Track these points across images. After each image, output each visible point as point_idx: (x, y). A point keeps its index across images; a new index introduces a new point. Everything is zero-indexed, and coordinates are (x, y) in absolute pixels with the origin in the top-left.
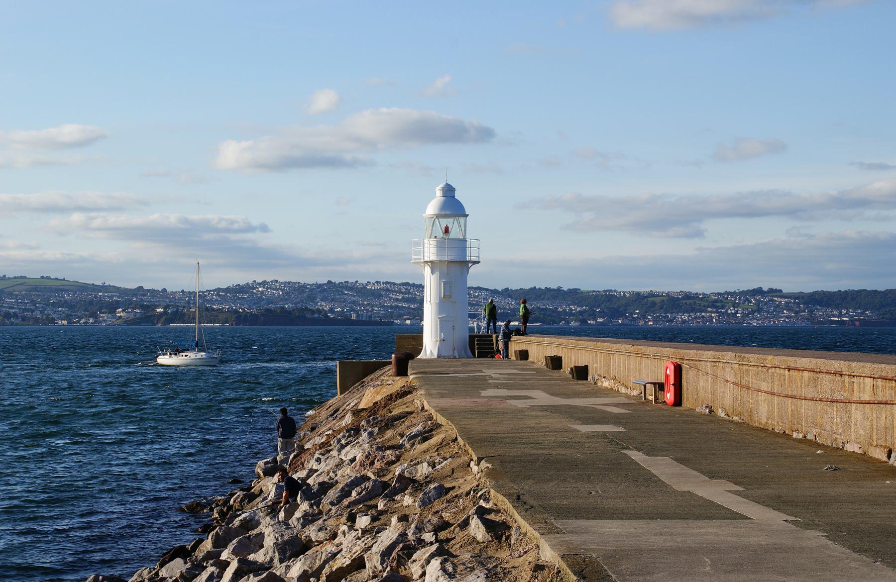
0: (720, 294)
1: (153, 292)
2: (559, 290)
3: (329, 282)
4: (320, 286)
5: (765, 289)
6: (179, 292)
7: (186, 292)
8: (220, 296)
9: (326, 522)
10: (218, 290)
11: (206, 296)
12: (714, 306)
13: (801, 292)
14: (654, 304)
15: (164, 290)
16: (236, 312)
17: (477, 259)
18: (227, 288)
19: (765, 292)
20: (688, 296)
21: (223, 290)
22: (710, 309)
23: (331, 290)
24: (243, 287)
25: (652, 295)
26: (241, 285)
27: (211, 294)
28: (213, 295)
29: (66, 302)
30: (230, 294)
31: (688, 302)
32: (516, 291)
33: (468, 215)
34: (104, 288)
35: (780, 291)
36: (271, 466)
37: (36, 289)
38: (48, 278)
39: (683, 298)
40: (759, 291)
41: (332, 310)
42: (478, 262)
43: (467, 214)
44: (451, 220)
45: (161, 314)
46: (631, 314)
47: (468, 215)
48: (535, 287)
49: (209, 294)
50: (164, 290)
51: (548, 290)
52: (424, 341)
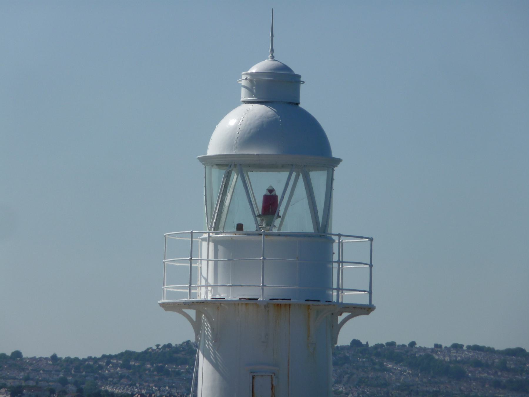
6: (46, 359)
7: (60, 359)
8: (129, 367)
9: (331, 169)
10: (128, 356)
11: (101, 367)
15: (17, 354)
17: (362, 299)
18: (146, 352)
23: (244, 187)
26: (173, 345)
27: (113, 364)
28: (115, 366)
30: (152, 364)
36: (138, 365)
42: (367, 309)
43: (365, 343)
44: (284, 175)
49: (108, 363)
50: (17, 354)
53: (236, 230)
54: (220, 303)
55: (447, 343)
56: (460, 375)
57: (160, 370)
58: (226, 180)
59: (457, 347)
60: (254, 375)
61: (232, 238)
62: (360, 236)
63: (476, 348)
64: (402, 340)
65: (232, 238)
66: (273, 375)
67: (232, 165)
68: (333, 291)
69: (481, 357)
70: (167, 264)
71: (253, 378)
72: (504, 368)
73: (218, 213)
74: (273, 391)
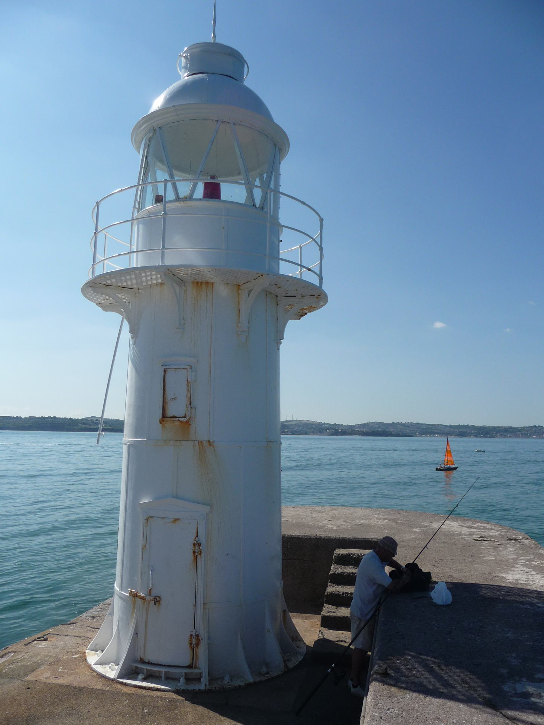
0: (522, 427)
1: (339, 425)
2: (468, 425)
3: (393, 422)
4: (390, 424)
5: (537, 426)
12: (520, 431)
13: (94, 417)
14: (499, 430)
16: (363, 431)
19: (537, 427)
20: (511, 428)
21: (360, 425)
22: (519, 432)
24: (366, 424)
25: (499, 427)
29: (313, 428)
31: (511, 430)
32: (454, 426)
33: (281, 241)
34: (324, 424)
35: (542, 426)
37: (305, 424)
38: (309, 420)
39: (510, 428)
40: (535, 426)
41: (394, 431)
43: (281, 240)
45: (340, 432)
46: (492, 434)
47: (281, 241)
48: (342, 424)
51: (464, 425)
52: (226, 45)
53: (154, 203)
54: (138, 289)
55: (407, 422)
56: (409, 427)
57: (364, 427)
58: (148, 150)
59: (408, 423)
60: (166, 369)
61: (149, 212)
62: (302, 200)
63: (411, 423)
64: (400, 422)
65: (149, 212)
66: (188, 367)
67: (521, 569)
68: (189, 182)
69: (412, 424)
70: (106, 263)
71: (165, 372)
72: (416, 426)
73: (141, 191)
74: (188, 388)
